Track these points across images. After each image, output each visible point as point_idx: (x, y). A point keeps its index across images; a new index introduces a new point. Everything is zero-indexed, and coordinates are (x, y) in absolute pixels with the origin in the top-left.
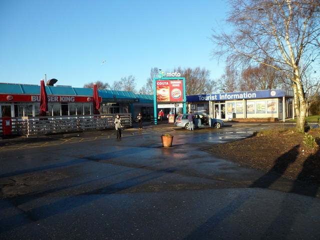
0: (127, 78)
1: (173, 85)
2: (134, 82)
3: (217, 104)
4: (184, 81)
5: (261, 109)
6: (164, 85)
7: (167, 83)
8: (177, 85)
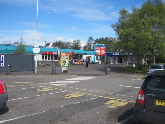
0: (76, 41)
1: (102, 49)
3: (163, 67)
4: (106, 47)
7: (99, 48)
8: (103, 49)
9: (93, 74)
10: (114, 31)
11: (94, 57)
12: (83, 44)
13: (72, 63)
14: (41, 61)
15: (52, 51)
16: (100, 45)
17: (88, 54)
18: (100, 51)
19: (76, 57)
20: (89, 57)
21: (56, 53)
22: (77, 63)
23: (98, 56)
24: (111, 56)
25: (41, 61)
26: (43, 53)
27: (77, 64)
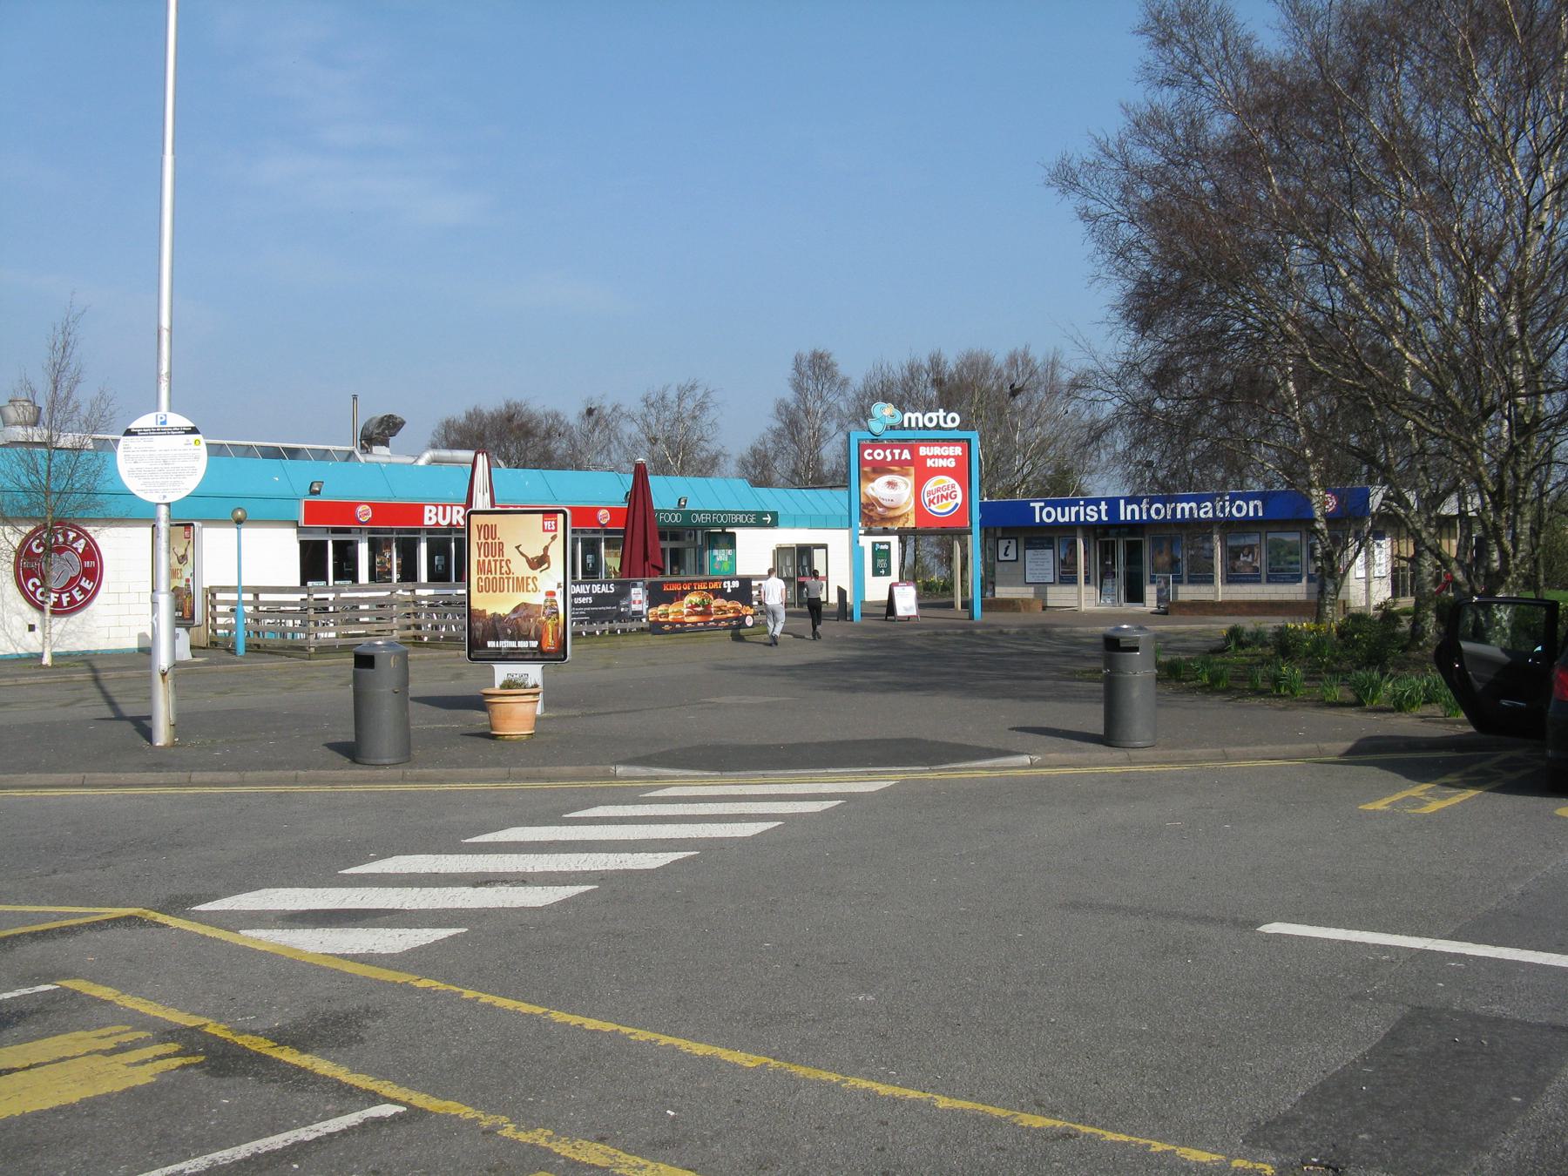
0: (672, 395)
1: (929, 463)
2: (706, 419)
4: (976, 444)
5: (1283, 565)
6: (894, 462)
7: (906, 455)
9: (874, 744)
10: (1081, 227)
11: (856, 552)
12: (742, 420)
13: (620, 617)
14: (297, 597)
15: (402, 494)
16: (913, 417)
17: (795, 523)
18: (910, 481)
19: (650, 545)
20: (805, 552)
21: (457, 516)
22: (679, 610)
23: (894, 540)
24: (1042, 536)
25: (297, 597)
26: (316, 511)
27: (678, 628)
